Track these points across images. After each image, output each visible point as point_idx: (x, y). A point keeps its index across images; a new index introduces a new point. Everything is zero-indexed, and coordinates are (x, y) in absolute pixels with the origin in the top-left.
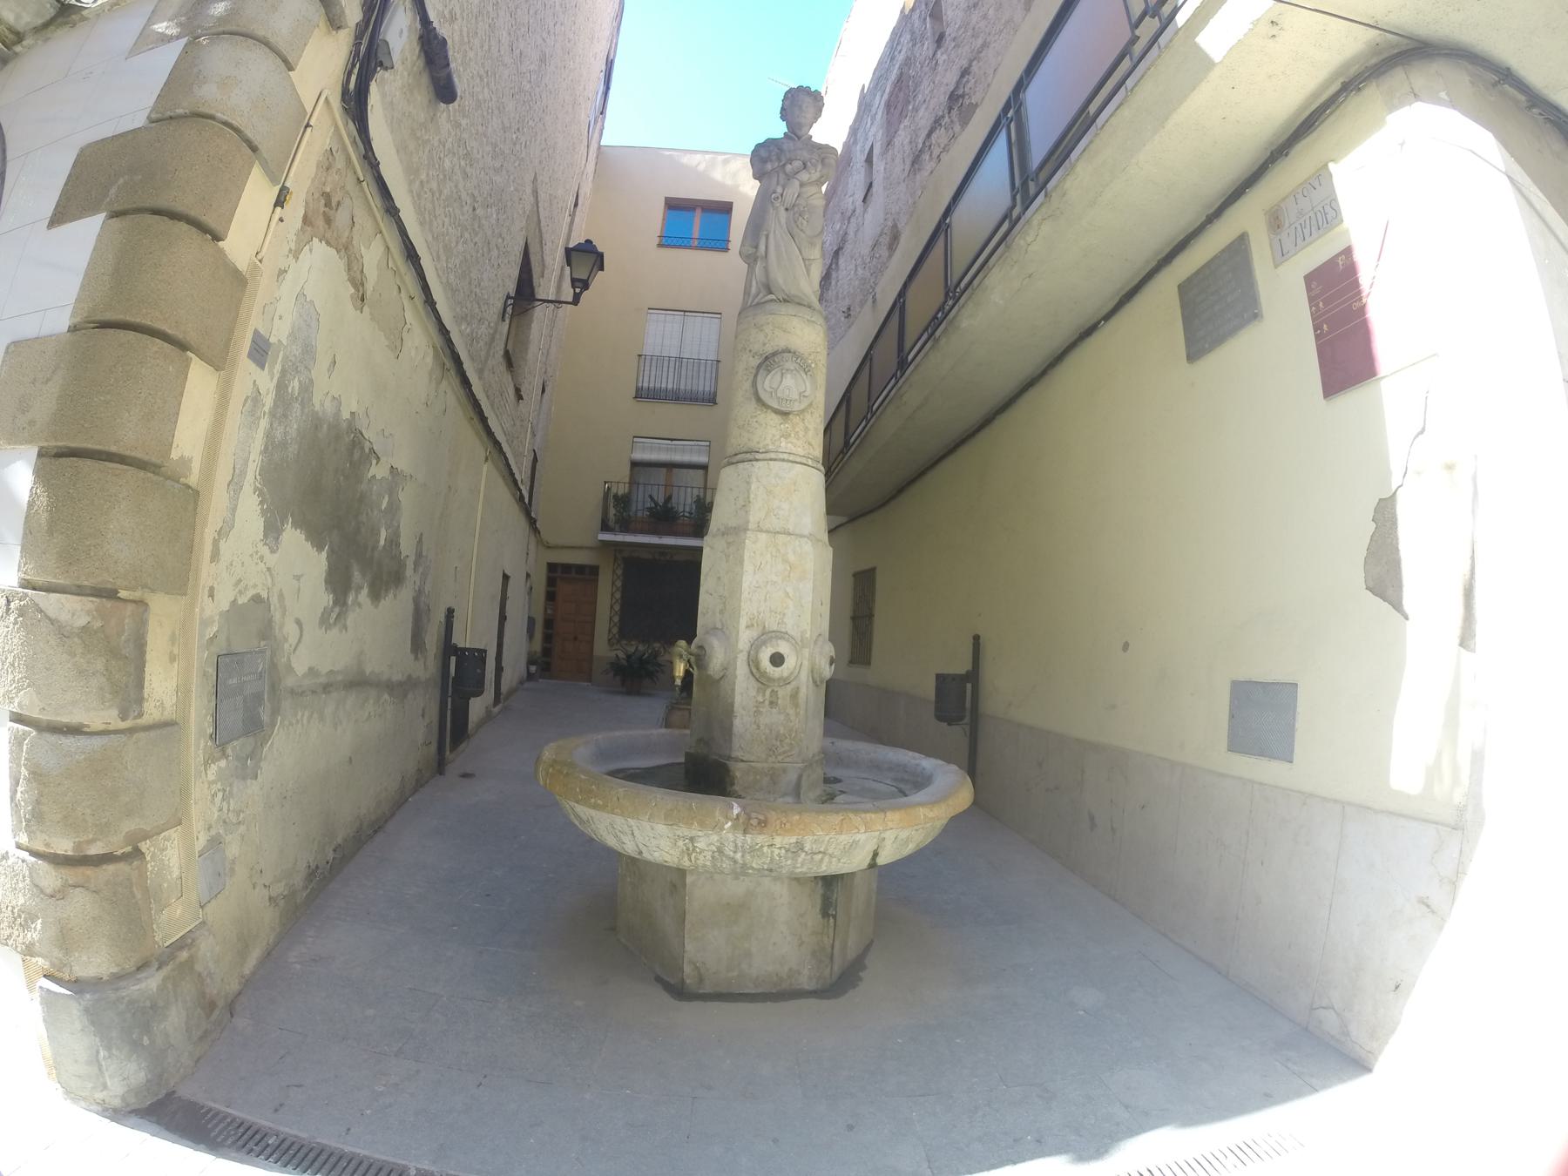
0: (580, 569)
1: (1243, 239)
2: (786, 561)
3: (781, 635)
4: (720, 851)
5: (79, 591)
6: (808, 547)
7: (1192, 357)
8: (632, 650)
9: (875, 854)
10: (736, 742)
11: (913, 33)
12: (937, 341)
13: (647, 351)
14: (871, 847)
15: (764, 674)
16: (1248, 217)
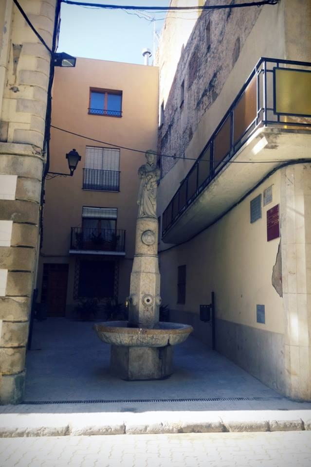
0: (59, 265)
1: (260, 195)
2: (149, 278)
3: (149, 295)
4: (138, 339)
5: (22, 296)
6: (154, 275)
7: (252, 222)
8: (85, 301)
9: (169, 340)
10: (139, 320)
11: (200, 30)
12: (194, 203)
13: (87, 167)
14: (168, 339)
15: (145, 304)
16: (260, 190)
